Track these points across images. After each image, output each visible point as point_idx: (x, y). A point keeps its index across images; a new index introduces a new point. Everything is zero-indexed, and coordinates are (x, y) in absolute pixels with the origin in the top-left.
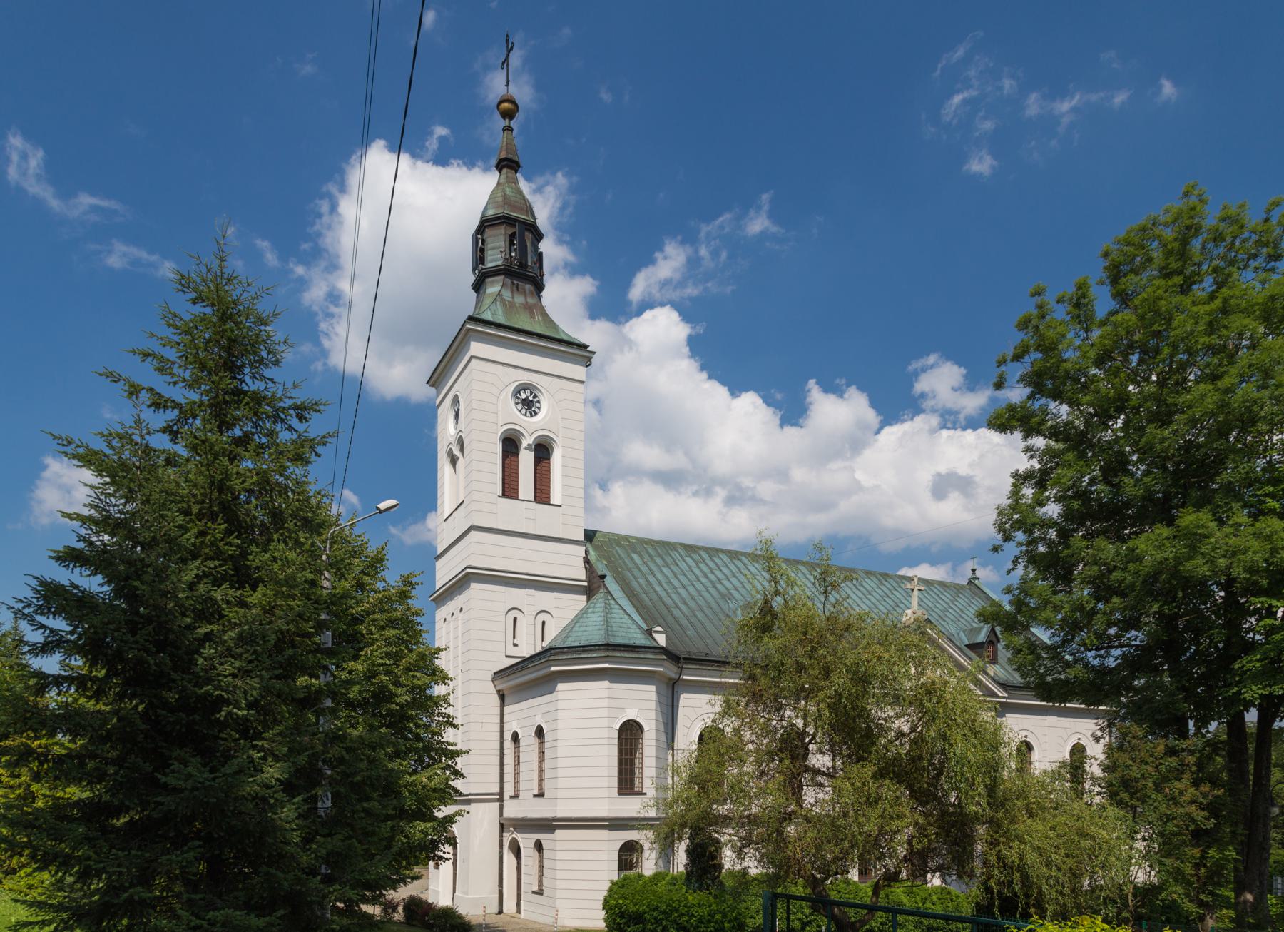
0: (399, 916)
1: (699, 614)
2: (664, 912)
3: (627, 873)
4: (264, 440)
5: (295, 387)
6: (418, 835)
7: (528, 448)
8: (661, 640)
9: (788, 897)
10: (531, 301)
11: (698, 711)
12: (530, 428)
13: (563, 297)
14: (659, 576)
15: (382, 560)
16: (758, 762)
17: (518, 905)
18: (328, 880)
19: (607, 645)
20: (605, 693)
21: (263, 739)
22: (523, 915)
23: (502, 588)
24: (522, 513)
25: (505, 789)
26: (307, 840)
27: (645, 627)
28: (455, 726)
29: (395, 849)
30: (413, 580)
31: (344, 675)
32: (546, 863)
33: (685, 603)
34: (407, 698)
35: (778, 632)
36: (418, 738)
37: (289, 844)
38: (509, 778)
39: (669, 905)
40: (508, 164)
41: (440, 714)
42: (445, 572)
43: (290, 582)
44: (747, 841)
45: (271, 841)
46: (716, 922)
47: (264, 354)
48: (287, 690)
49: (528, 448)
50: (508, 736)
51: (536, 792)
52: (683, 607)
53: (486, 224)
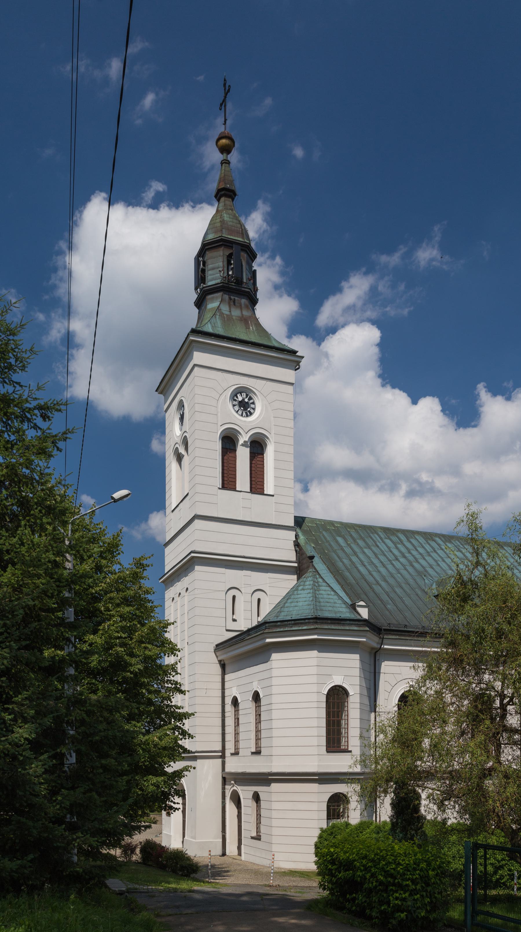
0: (137, 856)
1: (398, 590)
2: (373, 861)
3: (335, 821)
4: (13, 438)
5: (39, 389)
6: (151, 788)
7: (244, 445)
8: (364, 613)
9: (487, 847)
10: (246, 313)
11: (398, 677)
12: (246, 427)
13: (273, 312)
14: (361, 556)
15: (117, 546)
16: (458, 722)
17: (239, 848)
18: (73, 828)
19: (316, 618)
20: (314, 662)
21: (13, 703)
22: (243, 857)
23: (223, 570)
24: (240, 503)
25: (227, 747)
26: (54, 792)
27: (350, 602)
28: (182, 692)
29: (130, 801)
30: (145, 562)
31: (85, 647)
32: (263, 813)
33: (385, 581)
34: (139, 666)
35: (477, 601)
36: (150, 702)
37: (37, 796)
38: (230, 737)
39: (376, 854)
40: (225, 193)
41: (169, 681)
42: (173, 557)
43: (36, 563)
44: (448, 795)
45: (21, 793)
46: (421, 870)
47: (12, 361)
48: (34, 659)
49: (244, 445)
50: (228, 701)
51: (254, 750)
52: (383, 584)
53: (207, 247)
